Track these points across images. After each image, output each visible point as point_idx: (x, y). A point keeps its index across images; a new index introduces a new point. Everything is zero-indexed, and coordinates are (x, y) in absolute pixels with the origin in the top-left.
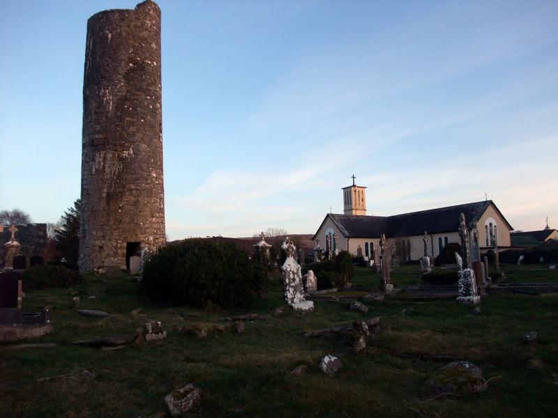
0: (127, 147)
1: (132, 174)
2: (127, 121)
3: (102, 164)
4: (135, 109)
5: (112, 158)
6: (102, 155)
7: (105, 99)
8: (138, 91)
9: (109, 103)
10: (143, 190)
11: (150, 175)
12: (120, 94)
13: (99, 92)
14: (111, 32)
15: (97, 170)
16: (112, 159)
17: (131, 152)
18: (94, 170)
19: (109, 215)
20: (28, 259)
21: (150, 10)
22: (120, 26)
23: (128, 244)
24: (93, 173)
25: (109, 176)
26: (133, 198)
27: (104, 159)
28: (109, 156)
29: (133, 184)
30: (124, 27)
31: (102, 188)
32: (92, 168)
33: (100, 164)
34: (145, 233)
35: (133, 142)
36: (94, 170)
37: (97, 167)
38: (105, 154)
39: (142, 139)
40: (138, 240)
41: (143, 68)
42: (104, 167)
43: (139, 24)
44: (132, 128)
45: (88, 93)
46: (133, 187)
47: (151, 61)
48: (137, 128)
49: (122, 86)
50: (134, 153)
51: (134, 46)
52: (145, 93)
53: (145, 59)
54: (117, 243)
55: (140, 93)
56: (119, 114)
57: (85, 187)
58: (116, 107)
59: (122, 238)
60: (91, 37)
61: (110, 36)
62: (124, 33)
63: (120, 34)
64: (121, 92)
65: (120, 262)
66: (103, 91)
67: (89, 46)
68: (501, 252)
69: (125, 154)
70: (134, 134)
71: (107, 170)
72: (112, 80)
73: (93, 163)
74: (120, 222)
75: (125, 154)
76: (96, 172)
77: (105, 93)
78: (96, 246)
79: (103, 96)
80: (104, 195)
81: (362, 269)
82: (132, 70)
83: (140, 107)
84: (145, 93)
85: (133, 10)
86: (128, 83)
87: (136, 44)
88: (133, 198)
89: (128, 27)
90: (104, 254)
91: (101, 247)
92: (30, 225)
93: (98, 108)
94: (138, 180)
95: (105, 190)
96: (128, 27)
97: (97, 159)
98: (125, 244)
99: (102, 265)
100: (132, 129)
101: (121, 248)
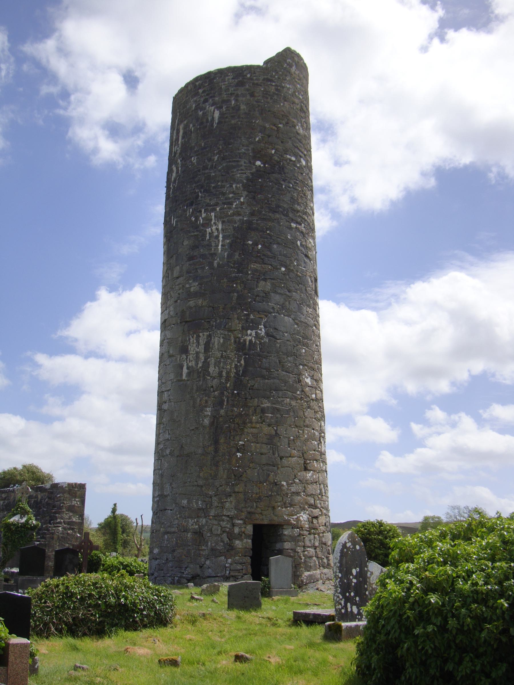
0: (252, 321)
1: (263, 377)
2: (255, 271)
3: (202, 357)
4: (267, 247)
5: (223, 345)
6: (203, 340)
7: (209, 230)
8: (274, 212)
9: (217, 237)
10: (288, 412)
11: (300, 381)
12: (237, 218)
13: (197, 219)
14: (219, 108)
15: (191, 371)
16: (223, 347)
17: (263, 332)
18: (185, 370)
19: (217, 465)
20: (51, 553)
21: (291, 66)
22: (237, 95)
23: (258, 529)
24: (184, 377)
25: (215, 382)
26: (266, 429)
27: (208, 347)
28: (217, 341)
29: (268, 398)
30: (243, 95)
31: (202, 409)
32: (181, 367)
33: (197, 358)
34: (291, 505)
35: (267, 313)
36: (185, 370)
37: (192, 364)
38: (210, 336)
39: (283, 307)
40: (276, 520)
41: (282, 169)
42: (206, 364)
43: (273, 89)
44: (262, 283)
45: (174, 222)
46: (266, 404)
47: (296, 157)
48: (272, 284)
49: (242, 203)
50: (267, 334)
51: (263, 130)
52: (287, 215)
53: (286, 152)
54: (233, 525)
55: (277, 216)
56: (237, 256)
57: (165, 407)
58: (231, 245)
59: (243, 515)
60: (180, 122)
61: (217, 114)
62: (243, 107)
63: (237, 108)
64: (239, 215)
65: (239, 567)
66: (204, 215)
67: (177, 139)
68: (232, 585)
69: (250, 335)
70: (266, 297)
71: (211, 369)
72: (224, 194)
73: (184, 356)
74: (238, 477)
75: (250, 335)
76: (188, 374)
77: (208, 220)
78: (186, 531)
79: (203, 225)
80: (206, 422)
81: (424, 579)
82: (259, 173)
83: (278, 244)
84: (287, 215)
85: (258, 67)
86: (254, 198)
87: (267, 125)
88: (266, 429)
89: (252, 95)
90: (205, 550)
91: (199, 534)
92: (55, 486)
93: (194, 247)
94: (276, 390)
95: (208, 411)
96: (252, 95)
97: (192, 349)
98: (249, 529)
99: (198, 571)
100: (264, 286)
101: (240, 536)
